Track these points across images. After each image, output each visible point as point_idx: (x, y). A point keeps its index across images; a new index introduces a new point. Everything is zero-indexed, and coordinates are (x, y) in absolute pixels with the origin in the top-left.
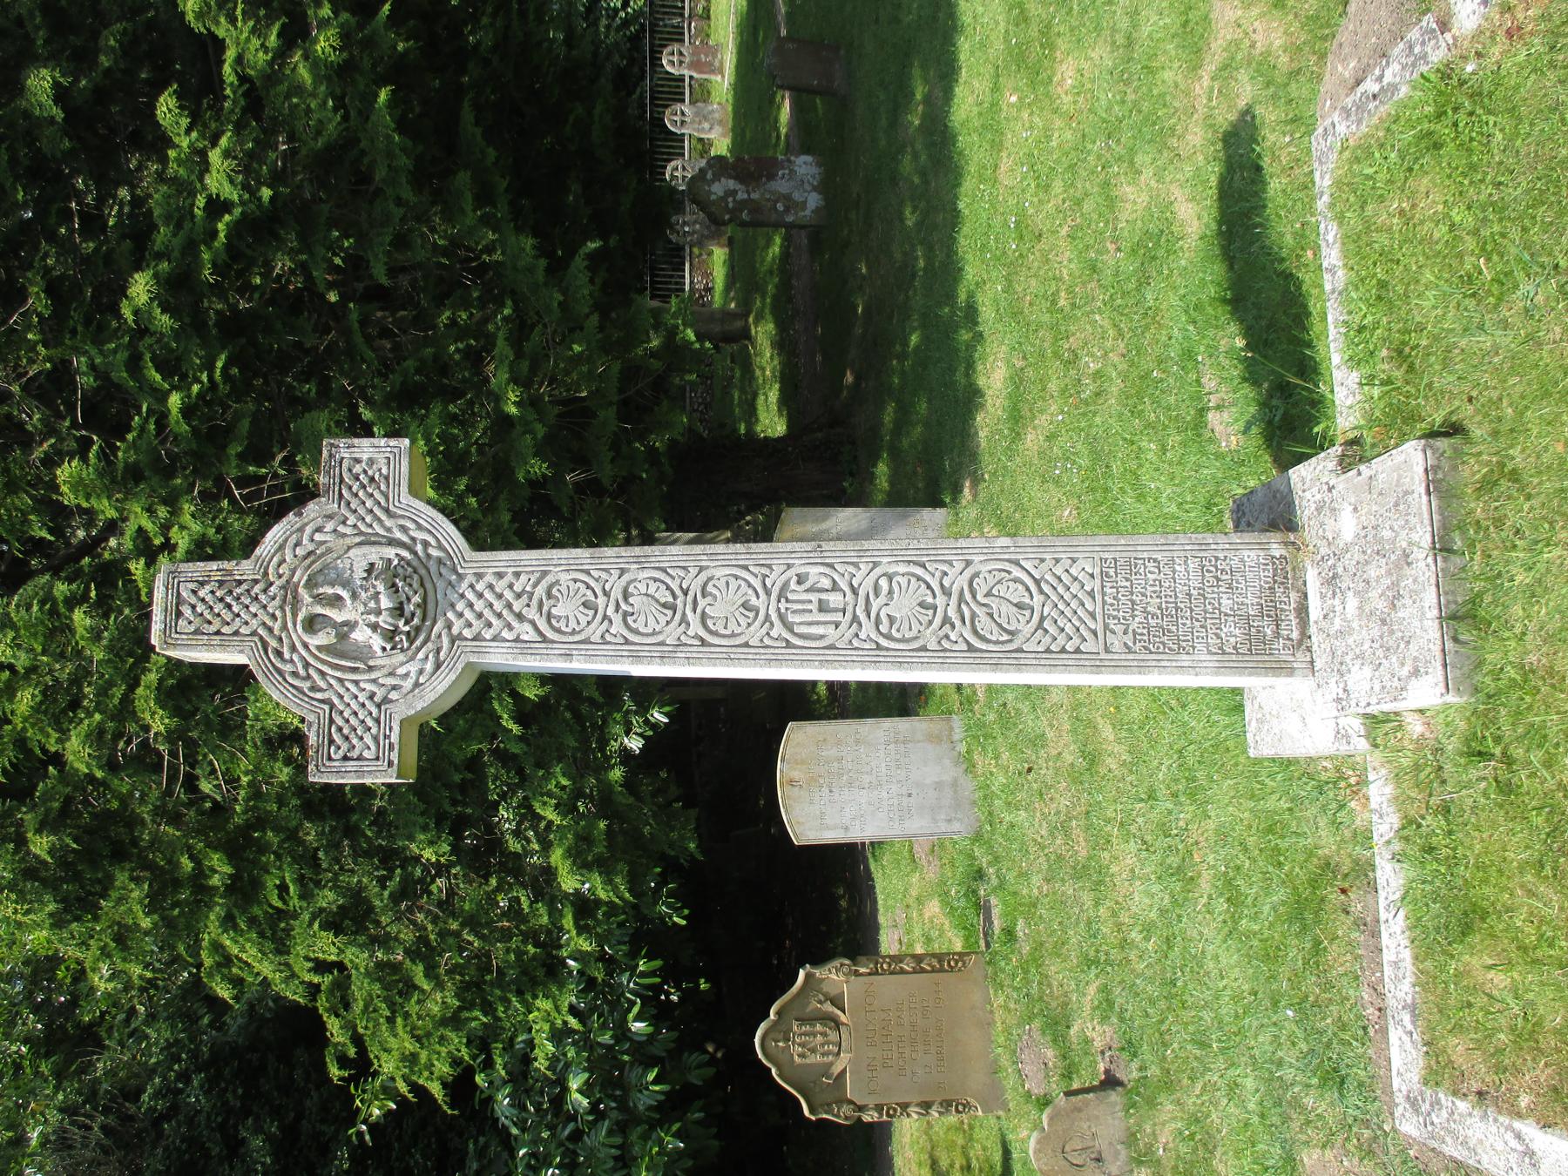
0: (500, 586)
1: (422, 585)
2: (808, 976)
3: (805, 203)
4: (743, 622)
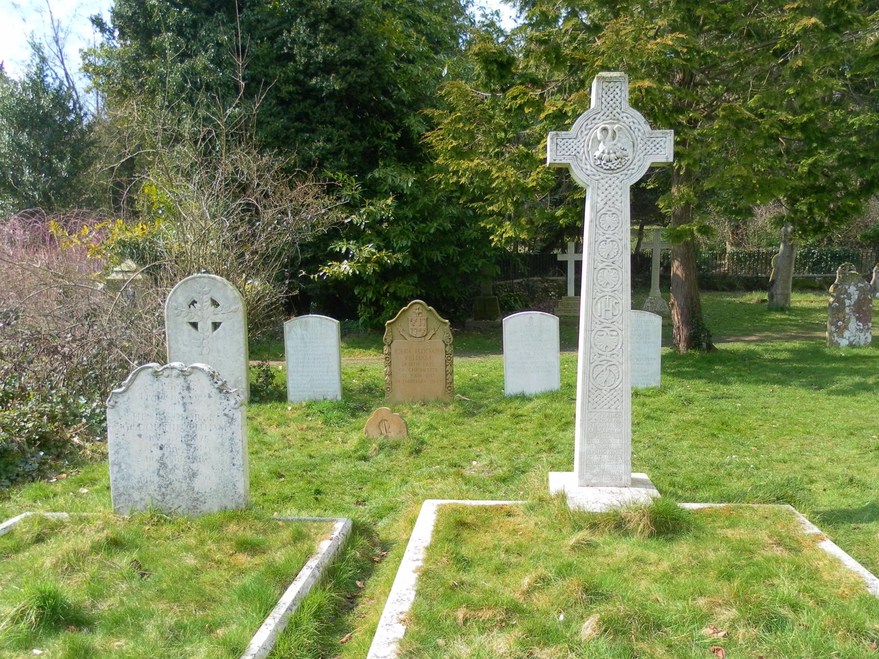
0: (617, 197)
1: (618, 168)
2: (446, 323)
3: (843, 337)
4: (602, 283)
